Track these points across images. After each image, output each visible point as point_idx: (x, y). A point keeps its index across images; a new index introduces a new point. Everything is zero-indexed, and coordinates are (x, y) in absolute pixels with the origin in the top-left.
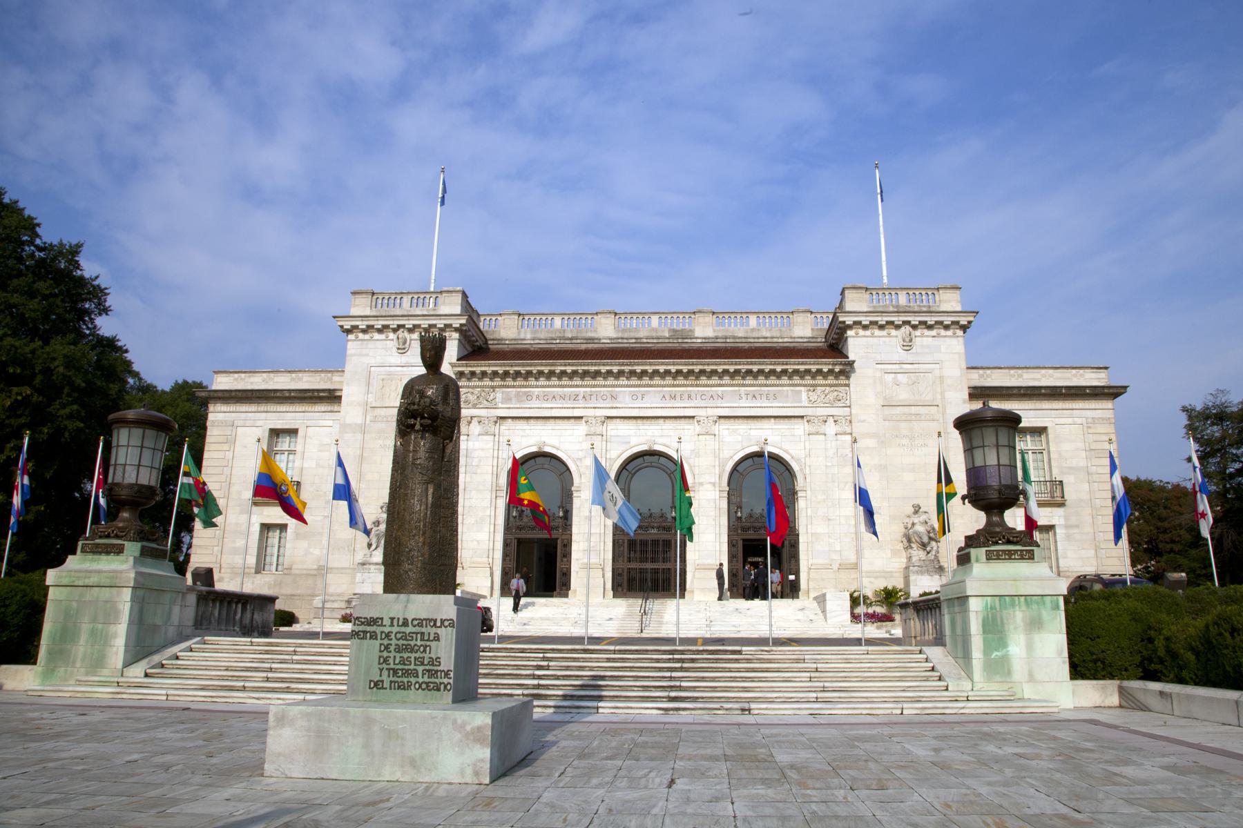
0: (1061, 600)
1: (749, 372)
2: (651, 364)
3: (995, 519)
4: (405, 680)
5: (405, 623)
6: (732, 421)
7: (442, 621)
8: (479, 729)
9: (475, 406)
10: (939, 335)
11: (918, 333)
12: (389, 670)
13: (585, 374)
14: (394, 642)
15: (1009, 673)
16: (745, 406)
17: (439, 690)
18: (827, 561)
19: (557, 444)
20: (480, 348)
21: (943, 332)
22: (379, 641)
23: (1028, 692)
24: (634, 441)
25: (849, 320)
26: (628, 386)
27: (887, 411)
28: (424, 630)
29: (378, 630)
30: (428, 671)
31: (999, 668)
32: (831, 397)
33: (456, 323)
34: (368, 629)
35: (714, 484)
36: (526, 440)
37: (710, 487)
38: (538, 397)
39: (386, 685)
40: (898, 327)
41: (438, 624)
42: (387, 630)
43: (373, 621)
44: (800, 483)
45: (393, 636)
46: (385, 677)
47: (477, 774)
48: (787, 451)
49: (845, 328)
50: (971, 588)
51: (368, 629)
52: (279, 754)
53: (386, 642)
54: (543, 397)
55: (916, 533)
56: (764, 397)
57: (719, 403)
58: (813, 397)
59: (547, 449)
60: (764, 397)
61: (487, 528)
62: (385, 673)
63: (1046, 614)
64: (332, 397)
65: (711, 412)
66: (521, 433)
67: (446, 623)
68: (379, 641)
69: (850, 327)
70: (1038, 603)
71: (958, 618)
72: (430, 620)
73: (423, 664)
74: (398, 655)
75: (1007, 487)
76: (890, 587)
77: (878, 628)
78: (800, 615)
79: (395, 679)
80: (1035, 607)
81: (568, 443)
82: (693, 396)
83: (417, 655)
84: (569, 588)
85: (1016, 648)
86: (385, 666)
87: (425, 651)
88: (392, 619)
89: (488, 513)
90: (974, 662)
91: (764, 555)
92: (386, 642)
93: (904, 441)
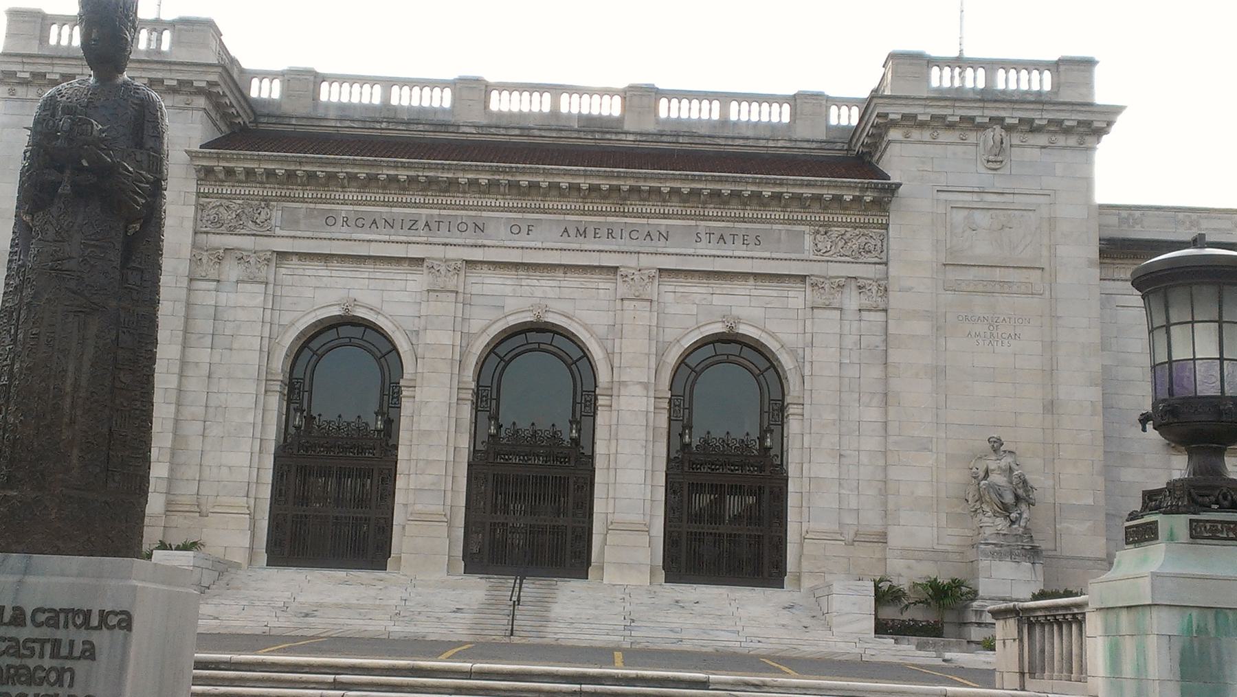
1: (716, 194)
2: (546, 173)
7: (104, 615)
9: (232, 231)
11: (1016, 139)
16: (706, 256)
20: (244, 129)
24: (511, 304)
26: (504, 209)
27: (952, 275)
28: (60, 634)
36: (318, 295)
37: (638, 390)
38: (346, 221)
40: (982, 127)
41: (95, 621)
49: (886, 124)
54: (353, 220)
55: (991, 486)
56: (739, 241)
57: (661, 246)
59: (360, 313)
60: (739, 241)
65: (645, 261)
67: (113, 620)
69: (894, 124)
72: (76, 612)
76: (944, 580)
77: (920, 647)
81: (389, 300)
82: (617, 233)
87: (59, 681)
91: (729, 517)
93: (981, 328)
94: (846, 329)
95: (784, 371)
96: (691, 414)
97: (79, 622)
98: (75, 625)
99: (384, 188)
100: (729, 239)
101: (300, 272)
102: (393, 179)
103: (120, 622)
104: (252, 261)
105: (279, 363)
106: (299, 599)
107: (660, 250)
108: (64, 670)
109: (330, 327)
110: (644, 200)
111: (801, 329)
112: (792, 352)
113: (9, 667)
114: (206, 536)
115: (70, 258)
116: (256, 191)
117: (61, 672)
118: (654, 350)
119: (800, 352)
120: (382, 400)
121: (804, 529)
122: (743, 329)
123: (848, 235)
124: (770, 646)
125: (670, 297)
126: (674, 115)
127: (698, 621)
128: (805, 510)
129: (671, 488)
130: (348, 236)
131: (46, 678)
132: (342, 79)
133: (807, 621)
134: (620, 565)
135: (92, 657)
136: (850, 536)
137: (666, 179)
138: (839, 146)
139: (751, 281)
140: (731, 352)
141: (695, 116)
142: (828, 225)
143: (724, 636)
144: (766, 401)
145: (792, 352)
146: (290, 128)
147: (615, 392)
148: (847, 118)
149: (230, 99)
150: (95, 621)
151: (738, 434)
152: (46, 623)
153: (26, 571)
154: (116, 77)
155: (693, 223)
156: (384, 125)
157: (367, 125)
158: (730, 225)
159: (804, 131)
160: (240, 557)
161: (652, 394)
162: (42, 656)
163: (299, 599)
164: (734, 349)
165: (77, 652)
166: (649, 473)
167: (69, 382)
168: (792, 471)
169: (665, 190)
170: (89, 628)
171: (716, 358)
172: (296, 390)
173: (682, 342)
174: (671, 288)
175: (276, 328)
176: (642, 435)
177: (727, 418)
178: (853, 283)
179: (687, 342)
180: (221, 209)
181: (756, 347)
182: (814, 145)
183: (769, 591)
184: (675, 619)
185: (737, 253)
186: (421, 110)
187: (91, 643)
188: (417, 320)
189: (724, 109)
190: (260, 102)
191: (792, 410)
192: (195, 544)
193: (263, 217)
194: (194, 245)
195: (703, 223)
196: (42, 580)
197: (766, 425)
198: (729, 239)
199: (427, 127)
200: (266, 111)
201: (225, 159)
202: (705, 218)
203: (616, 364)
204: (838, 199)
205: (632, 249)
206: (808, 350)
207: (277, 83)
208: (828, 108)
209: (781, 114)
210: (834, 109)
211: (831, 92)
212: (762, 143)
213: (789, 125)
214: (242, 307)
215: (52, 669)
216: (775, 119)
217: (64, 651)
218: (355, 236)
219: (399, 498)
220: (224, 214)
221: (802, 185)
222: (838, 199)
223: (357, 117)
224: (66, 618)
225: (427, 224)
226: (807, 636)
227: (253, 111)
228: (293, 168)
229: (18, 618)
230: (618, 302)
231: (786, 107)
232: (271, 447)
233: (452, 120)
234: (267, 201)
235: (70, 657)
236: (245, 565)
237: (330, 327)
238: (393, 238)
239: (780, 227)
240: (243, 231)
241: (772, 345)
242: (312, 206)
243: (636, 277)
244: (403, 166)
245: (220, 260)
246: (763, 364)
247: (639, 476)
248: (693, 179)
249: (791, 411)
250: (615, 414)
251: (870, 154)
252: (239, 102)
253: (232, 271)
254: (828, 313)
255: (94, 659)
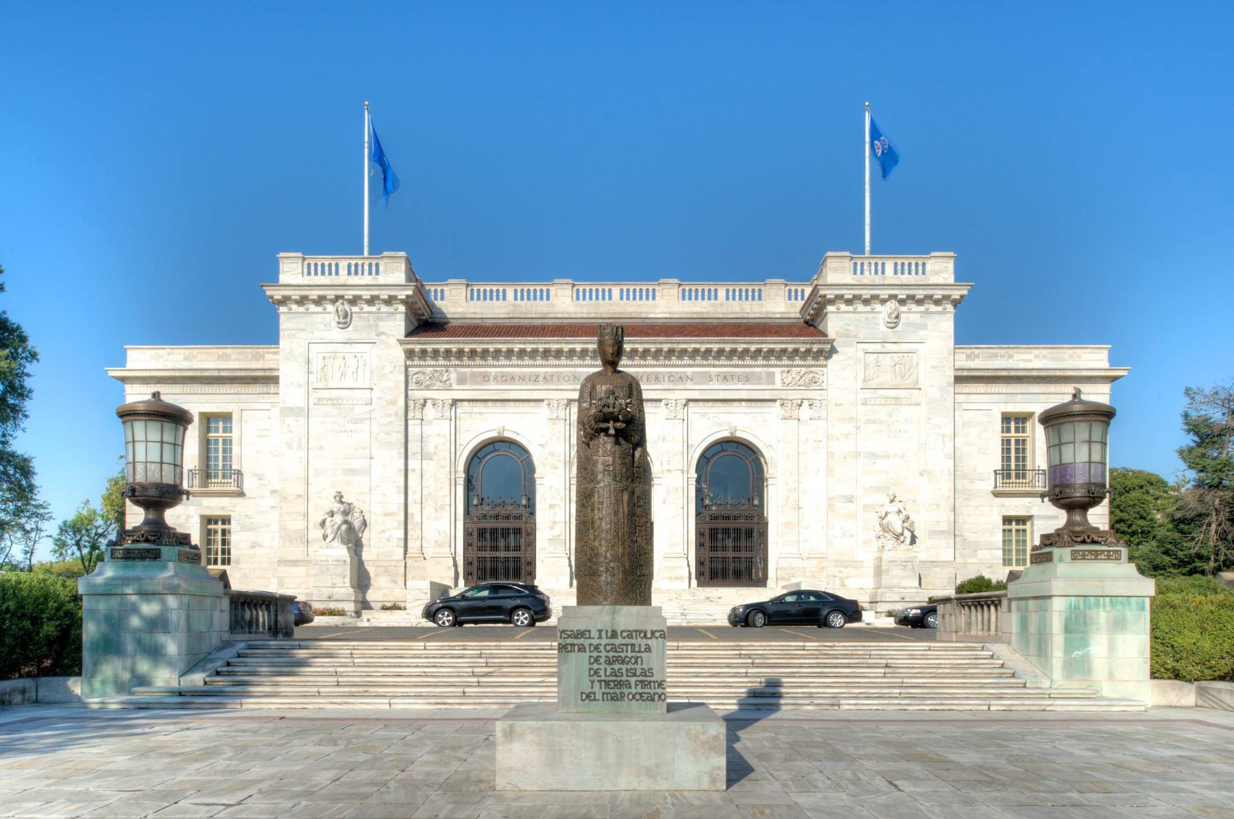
0: (1148, 601)
3: (1077, 518)
4: (618, 691)
6: (701, 404)
7: (653, 633)
8: (716, 738)
9: (428, 388)
10: (927, 312)
12: (600, 681)
13: (546, 354)
14: (603, 654)
15: (1089, 671)
17: (653, 700)
21: (933, 308)
22: (588, 654)
23: (1107, 690)
25: (830, 294)
28: (634, 641)
29: (586, 642)
30: (641, 682)
31: (1078, 666)
33: (402, 294)
34: (575, 641)
36: (480, 426)
39: (599, 696)
40: (884, 302)
41: (649, 635)
42: (595, 642)
43: (581, 634)
45: (602, 648)
46: (596, 688)
47: (713, 781)
50: (1057, 587)
51: (575, 641)
52: (511, 769)
53: (595, 654)
57: (690, 385)
59: (507, 434)
61: (446, 515)
62: (597, 685)
63: (1130, 615)
64: (269, 380)
67: (657, 634)
68: (588, 654)
70: (1123, 604)
71: (1034, 619)
73: (635, 675)
74: (609, 668)
75: (1096, 485)
79: (608, 690)
80: (1120, 607)
83: (629, 667)
85: (1098, 646)
86: (595, 678)
87: (636, 662)
88: (600, 631)
90: (1054, 660)
92: (595, 654)
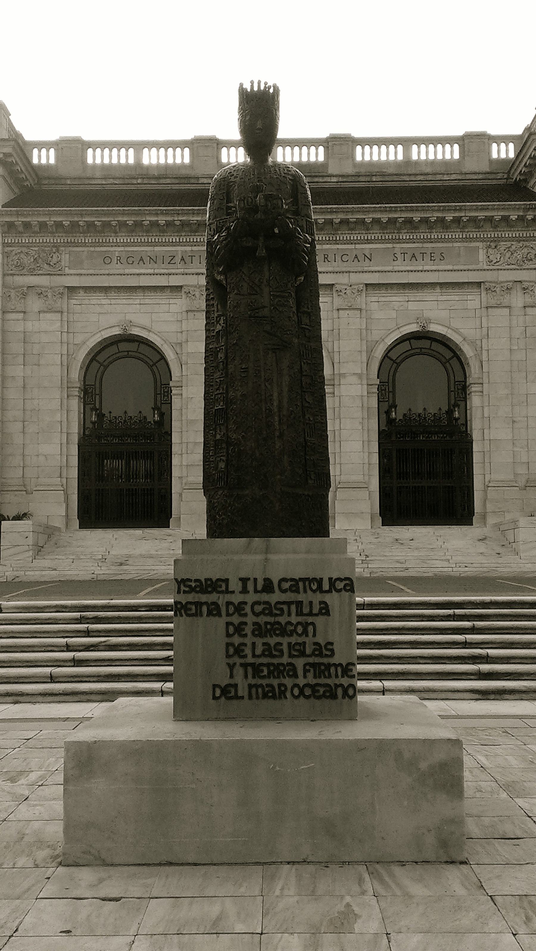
4: (275, 682)
5: (268, 586)
14: (250, 619)
16: (402, 271)
17: (334, 697)
18: (512, 477)
19: (148, 324)
28: (301, 597)
29: (221, 600)
32: (519, 255)
34: (204, 598)
35: (360, 376)
38: (119, 260)
41: (326, 587)
42: (237, 599)
44: (474, 371)
45: (248, 609)
46: (239, 679)
48: (456, 331)
51: (204, 598)
53: (236, 619)
56: (427, 258)
57: (366, 265)
58: (494, 256)
59: (136, 331)
60: (427, 258)
62: (239, 672)
65: (355, 278)
66: (98, 309)
67: (340, 585)
73: (303, 654)
74: (259, 642)
78: (482, 547)
82: (331, 257)
83: (293, 640)
84: (169, 515)
86: (238, 660)
87: (305, 632)
89: (58, 417)
92: (236, 619)
94: (514, 322)
95: (466, 358)
96: (394, 395)
97: (314, 587)
98: (311, 589)
99: (148, 231)
100: (419, 257)
101: (87, 302)
102: (154, 224)
103: (345, 586)
104: (49, 295)
105: (76, 374)
106: (113, 552)
107: (366, 269)
108: (308, 624)
109: (112, 344)
110: (352, 229)
111: (478, 323)
112: (472, 343)
113: (266, 623)
114: (32, 508)
115: (265, 307)
116: (49, 239)
117: (305, 626)
118: (365, 347)
119: (478, 343)
120: (156, 399)
121: (487, 480)
122: (433, 328)
123: (513, 247)
124: (475, 570)
125: (374, 306)
126: (367, 158)
127: (416, 553)
128: (487, 465)
129: (383, 454)
130: (121, 272)
131: (295, 631)
132: (103, 145)
133: (499, 550)
134: (348, 515)
135: (328, 613)
136: (522, 482)
137: (368, 211)
138: (499, 176)
139: (438, 290)
140: (427, 348)
141: (384, 158)
142: (497, 240)
143: (438, 564)
144: (452, 382)
145: (472, 343)
146: (64, 188)
147: (336, 382)
148: (506, 152)
149: (20, 167)
150: (326, 587)
151: (432, 410)
152: (290, 589)
153: (267, 551)
154: (267, 160)
155: (390, 246)
156: (139, 181)
157: (127, 181)
158: (420, 245)
159: (471, 166)
160: (59, 523)
161: (365, 382)
162: (289, 615)
163: (113, 552)
164: (426, 343)
165: (316, 610)
166: (366, 443)
167: (275, 404)
168: (476, 435)
169: (368, 221)
170: (322, 592)
171: (412, 352)
172: (90, 394)
173: (386, 341)
174: (374, 299)
175: (71, 346)
176: (359, 414)
177: (424, 399)
178: (519, 285)
179: (390, 341)
180: (22, 256)
181: (443, 341)
182: (481, 176)
183: (464, 528)
184: (398, 553)
185: (426, 268)
186: (167, 167)
187: (325, 603)
188: (179, 334)
189: (407, 152)
190: (40, 167)
191: (474, 388)
192: (25, 515)
193: (55, 260)
194: (4, 285)
195: (398, 245)
196: (282, 557)
197: (453, 402)
198: (419, 257)
199: (174, 181)
200: (46, 175)
201: (23, 215)
202: (399, 241)
203: (336, 360)
204: (505, 219)
205: (344, 269)
206: (484, 341)
207: (52, 151)
208: (490, 146)
209: (452, 153)
210: (494, 146)
211: (493, 131)
212: (439, 177)
213: (459, 162)
214: (46, 332)
215: (299, 623)
216: (448, 157)
217: (306, 610)
218: (127, 271)
219: (175, 473)
220: (26, 260)
221: (477, 209)
222: (505, 219)
223: (117, 175)
224: (304, 584)
225: (183, 259)
226: (500, 561)
227: (37, 175)
228: (76, 219)
229: (268, 586)
230: (335, 312)
231: (456, 147)
232: (75, 439)
233: (192, 173)
234: (57, 246)
235: (311, 614)
236: (63, 529)
237: (112, 344)
238: (156, 271)
239: (458, 244)
240: (40, 272)
241: (456, 338)
242: (92, 249)
243: (348, 292)
244: (162, 213)
245: (24, 295)
246: (448, 354)
247: (357, 446)
248: (391, 210)
249: (473, 389)
250: (337, 399)
251: (526, 181)
252: (27, 170)
253: (34, 304)
254: (498, 311)
255: (329, 615)
